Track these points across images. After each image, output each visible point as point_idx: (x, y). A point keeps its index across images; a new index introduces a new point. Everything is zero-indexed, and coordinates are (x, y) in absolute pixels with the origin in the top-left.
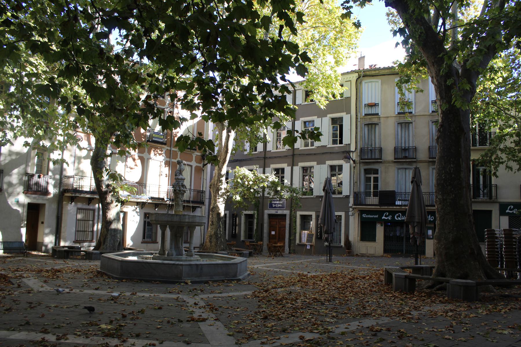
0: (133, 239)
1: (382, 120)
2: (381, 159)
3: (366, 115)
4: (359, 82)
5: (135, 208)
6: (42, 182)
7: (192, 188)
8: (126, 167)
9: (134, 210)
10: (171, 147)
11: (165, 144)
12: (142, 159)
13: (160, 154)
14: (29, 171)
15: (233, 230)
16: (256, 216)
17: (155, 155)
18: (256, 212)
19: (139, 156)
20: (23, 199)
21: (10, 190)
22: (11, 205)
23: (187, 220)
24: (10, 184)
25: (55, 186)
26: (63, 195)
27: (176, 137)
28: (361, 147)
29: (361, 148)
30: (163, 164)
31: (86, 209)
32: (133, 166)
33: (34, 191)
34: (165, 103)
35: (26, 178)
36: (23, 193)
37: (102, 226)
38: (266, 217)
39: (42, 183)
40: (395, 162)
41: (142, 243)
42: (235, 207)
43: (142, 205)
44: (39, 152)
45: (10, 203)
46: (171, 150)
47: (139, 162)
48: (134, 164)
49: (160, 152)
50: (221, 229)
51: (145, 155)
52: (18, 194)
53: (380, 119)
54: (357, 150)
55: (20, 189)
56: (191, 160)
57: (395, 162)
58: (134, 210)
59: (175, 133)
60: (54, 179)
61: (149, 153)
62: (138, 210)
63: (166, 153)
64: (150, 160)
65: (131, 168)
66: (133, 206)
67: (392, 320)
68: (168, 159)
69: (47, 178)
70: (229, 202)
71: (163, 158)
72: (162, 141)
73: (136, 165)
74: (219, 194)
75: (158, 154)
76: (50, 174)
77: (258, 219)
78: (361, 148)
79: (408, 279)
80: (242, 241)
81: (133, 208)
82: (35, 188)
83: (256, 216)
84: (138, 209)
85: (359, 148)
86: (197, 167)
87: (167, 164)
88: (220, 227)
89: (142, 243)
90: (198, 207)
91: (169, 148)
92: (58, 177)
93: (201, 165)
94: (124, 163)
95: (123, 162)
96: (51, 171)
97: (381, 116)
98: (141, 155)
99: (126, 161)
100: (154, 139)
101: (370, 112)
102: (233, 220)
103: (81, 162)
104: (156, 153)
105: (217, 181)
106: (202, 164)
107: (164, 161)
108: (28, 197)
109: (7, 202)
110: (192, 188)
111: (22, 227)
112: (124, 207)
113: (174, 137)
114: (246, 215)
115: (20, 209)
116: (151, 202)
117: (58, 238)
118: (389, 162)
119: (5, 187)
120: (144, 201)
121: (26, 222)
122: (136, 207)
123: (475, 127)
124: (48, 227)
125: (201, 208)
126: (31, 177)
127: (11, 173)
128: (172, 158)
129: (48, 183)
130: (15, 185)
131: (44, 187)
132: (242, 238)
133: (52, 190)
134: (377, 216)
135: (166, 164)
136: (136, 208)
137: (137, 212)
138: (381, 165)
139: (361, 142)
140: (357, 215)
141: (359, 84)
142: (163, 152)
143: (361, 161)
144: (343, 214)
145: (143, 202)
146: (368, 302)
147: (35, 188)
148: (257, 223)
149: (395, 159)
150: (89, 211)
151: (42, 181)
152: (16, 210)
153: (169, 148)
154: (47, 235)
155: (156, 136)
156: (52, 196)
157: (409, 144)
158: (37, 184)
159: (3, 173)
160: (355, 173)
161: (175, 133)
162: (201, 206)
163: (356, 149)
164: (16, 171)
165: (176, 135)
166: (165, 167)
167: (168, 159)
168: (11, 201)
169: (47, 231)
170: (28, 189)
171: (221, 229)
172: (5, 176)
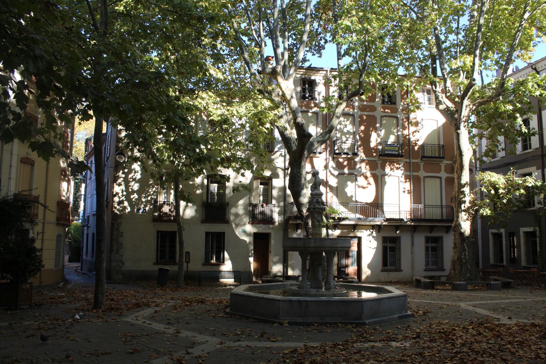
0: (369, 266)
5: (370, 233)
6: (268, 211)
7: (444, 204)
8: (357, 187)
9: (369, 235)
10: (410, 159)
11: (402, 156)
12: (375, 176)
13: (398, 168)
14: (254, 202)
15: (511, 253)
16: (538, 233)
17: (391, 169)
18: (537, 228)
19: (371, 174)
20: (249, 228)
21: (237, 221)
22: (239, 236)
23: (312, 245)
24: (237, 215)
25: (279, 214)
26: (288, 222)
27: (416, 146)
30: (403, 179)
32: (365, 185)
33: (259, 221)
34: (398, 110)
35: (251, 209)
36: (249, 223)
38: (522, 234)
39: (266, 211)
41: (382, 271)
42: (489, 223)
43: (378, 228)
44: (261, 181)
45: (237, 233)
46: (410, 162)
47: (371, 180)
48: (366, 182)
49: (398, 166)
50: (467, 253)
51: (378, 172)
52: (245, 224)
55: (246, 219)
56: (439, 171)
58: (369, 235)
59: (414, 142)
60: (279, 206)
61: (383, 169)
62: (374, 234)
63: (404, 166)
64: (386, 177)
65: (364, 188)
66: (368, 230)
68: (408, 173)
69: (270, 207)
70: (474, 218)
71: (402, 172)
72: (397, 153)
73: (369, 184)
74: (461, 208)
75: (395, 169)
76: (274, 202)
77: (541, 237)
80: (492, 265)
81: (368, 232)
82: (260, 217)
83: (538, 233)
84: (374, 233)
87: (407, 177)
88: (464, 250)
89: (382, 271)
91: (408, 160)
92: (282, 204)
94: (354, 183)
95: (352, 182)
96: (275, 199)
98: (374, 172)
99: (356, 180)
100: (386, 152)
102: (510, 240)
103: (385, 183)
104: (393, 167)
105: (458, 193)
107: (403, 176)
108: (254, 226)
109: (235, 233)
110: (444, 204)
111: (250, 256)
112: (358, 231)
113: (413, 147)
114: (526, 233)
115: (247, 239)
116: (387, 223)
117: (285, 268)
119: (232, 218)
120: (379, 223)
121: (253, 252)
122: (371, 231)
123: (365, 115)
124: (276, 255)
126: (255, 207)
127: (236, 205)
128: (413, 171)
129: (272, 211)
130: (242, 216)
131: (268, 216)
132: (523, 263)
133: (277, 218)
135: (406, 178)
136: (372, 232)
137: (373, 237)
142: (401, 166)
145: (377, 225)
146: (431, 341)
147: (260, 217)
148: (541, 244)
151: (267, 209)
152: (243, 240)
153: (408, 160)
154: (275, 263)
155: (389, 148)
156: (277, 224)
158: (263, 213)
159: (228, 205)
161: (414, 142)
164: (241, 202)
165: (416, 144)
166: (406, 182)
167: (408, 173)
168: (238, 232)
169: (276, 259)
170: (254, 220)
171: (467, 253)
172: (231, 209)
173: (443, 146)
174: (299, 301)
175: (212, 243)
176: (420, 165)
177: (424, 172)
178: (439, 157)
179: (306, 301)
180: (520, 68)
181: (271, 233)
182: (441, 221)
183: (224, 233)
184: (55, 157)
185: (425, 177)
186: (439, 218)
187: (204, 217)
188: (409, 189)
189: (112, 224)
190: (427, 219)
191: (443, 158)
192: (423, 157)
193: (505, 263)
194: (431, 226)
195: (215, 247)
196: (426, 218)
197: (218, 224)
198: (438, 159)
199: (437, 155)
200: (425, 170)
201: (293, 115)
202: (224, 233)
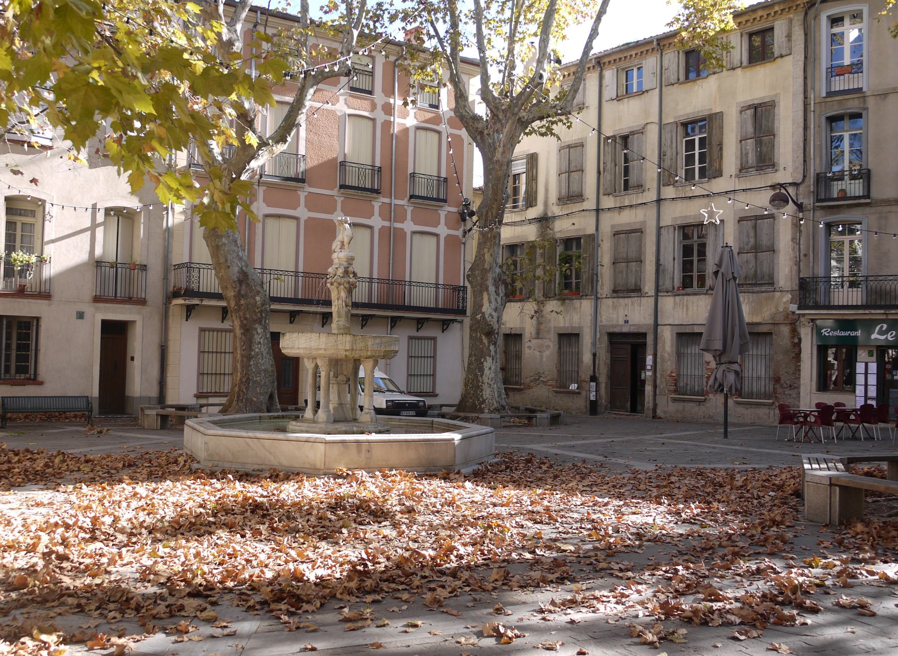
1: (871, 103)
2: (868, 197)
4: (813, 16)
28: (818, 171)
29: (818, 175)
31: (218, 330)
37: (645, 361)
53: (865, 102)
54: (807, 179)
67: (870, 578)
78: (818, 175)
79: (837, 489)
85: (812, 175)
86: (448, 238)
90: (453, 321)
91: (387, 200)
93: (459, 233)
97: (869, 93)
106: (461, 230)
125: (461, 322)
138: (867, 210)
139: (818, 160)
141: (813, 22)
143: (817, 204)
150: (224, 333)
153: (387, 200)
157: (601, 78)
162: (459, 318)
163: (804, 176)
173: (446, 179)
174: (357, 442)
175: (9, 337)
176: (406, 210)
177: (412, 223)
178: (438, 200)
179: (369, 442)
180: (475, 31)
182: (435, 310)
183: (38, 319)
185: (414, 233)
186: (432, 305)
188: (47, 223)
190: (301, 299)
191: (445, 201)
192: (411, 197)
194: (363, 316)
195: (14, 346)
196: (201, 290)
197: (26, 300)
199: (368, 186)
200: (415, 221)
202: (38, 319)
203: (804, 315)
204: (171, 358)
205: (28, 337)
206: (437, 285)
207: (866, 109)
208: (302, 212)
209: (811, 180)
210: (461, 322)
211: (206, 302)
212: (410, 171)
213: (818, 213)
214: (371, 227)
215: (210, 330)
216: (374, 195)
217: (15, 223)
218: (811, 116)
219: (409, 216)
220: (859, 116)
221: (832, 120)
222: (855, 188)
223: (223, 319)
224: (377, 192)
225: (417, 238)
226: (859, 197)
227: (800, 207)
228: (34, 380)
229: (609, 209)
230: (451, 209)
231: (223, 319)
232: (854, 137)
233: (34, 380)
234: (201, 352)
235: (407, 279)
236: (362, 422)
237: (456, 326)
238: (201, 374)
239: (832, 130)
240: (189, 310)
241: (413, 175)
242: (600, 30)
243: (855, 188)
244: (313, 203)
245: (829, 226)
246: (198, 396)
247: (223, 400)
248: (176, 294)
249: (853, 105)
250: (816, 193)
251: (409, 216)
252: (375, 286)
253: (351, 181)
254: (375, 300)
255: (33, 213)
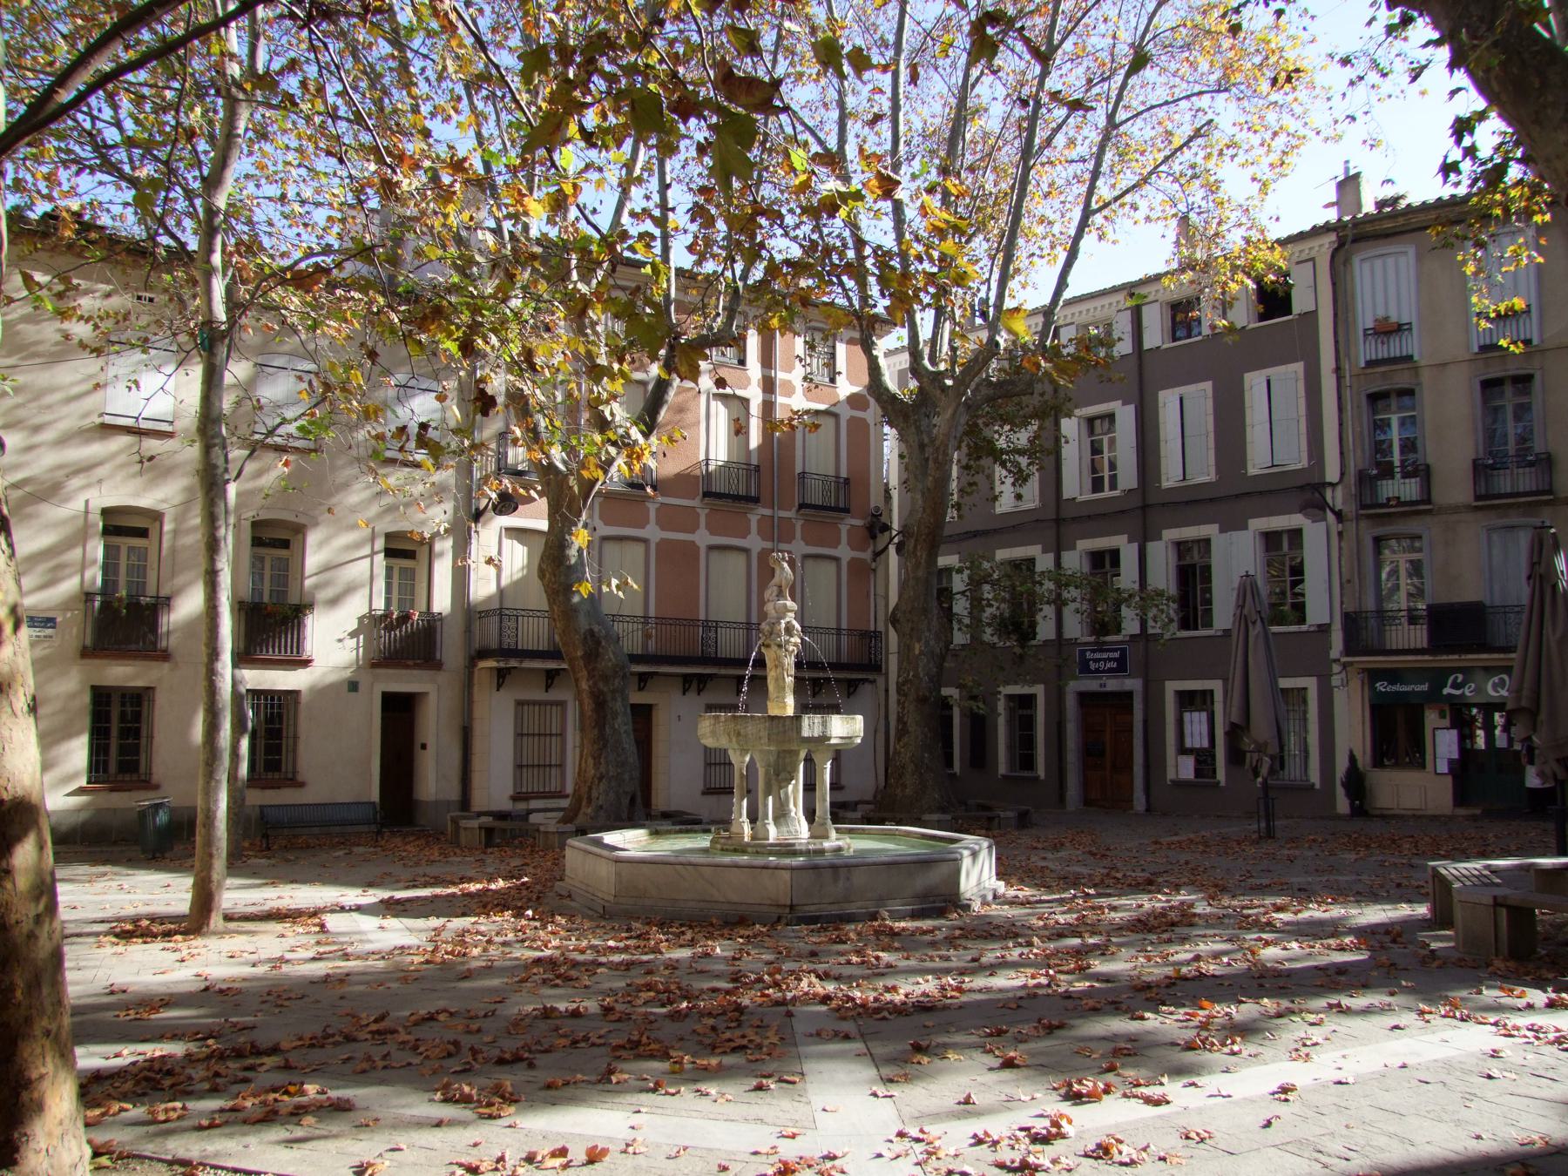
1: (1426, 377)
2: (1428, 501)
3: (1370, 364)
28: (1361, 467)
40: (1477, 508)
41: (704, 793)
53: (1417, 375)
54: (1346, 477)
57: (1477, 508)
86: (853, 563)
89: (704, 793)
91: (767, 512)
93: (867, 555)
97: (1423, 363)
101: (1383, 353)
106: (870, 551)
114: (1010, 697)
118: (1456, 509)
134: (1425, 687)
138: (1428, 519)
139: (1359, 452)
140: (1356, 684)
144: (1310, 683)
149: (1478, 498)
153: (767, 512)
160: (1345, 552)
162: (871, 677)
163: (1342, 474)
173: (847, 481)
178: (836, 509)
181: (425, 694)
184: (1452, 72)
185: (711, 548)
187: (242, 646)
189: (1022, 904)
191: (847, 510)
192: (802, 506)
193: (957, 767)
198: (834, 514)
201: (710, 346)
203: (1351, 664)
204: (478, 745)
205: (137, 717)
206: (839, 630)
207: (1419, 384)
208: (653, 532)
209: (1351, 478)
210: (873, 682)
211: (528, 664)
212: (798, 470)
213: (1363, 524)
214: (836, 559)
215: (528, 703)
216: (751, 505)
217: (118, 548)
218: (1347, 394)
219: (703, 520)
220: (1410, 392)
221: (1374, 398)
222: (1408, 489)
223: (548, 688)
224: (756, 500)
225: (715, 555)
226: (1412, 503)
227: (1339, 515)
228: (294, 782)
229: (1074, 519)
230: (851, 523)
231: (548, 688)
232: (1402, 422)
233: (294, 782)
234: (519, 735)
235: (702, 617)
236: (1384, 817)
237: (868, 687)
238: (519, 767)
239: (1375, 412)
240: (502, 676)
241: (803, 475)
242: (1069, 280)
243: (1408, 489)
244: (668, 518)
245: (1378, 541)
246: (516, 798)
247: (565, 803)
248: (483, 654)
249: (1402, 380)
250: (1360, 495)
251: (703, 520)
252: (844, 639)
253: (815, 498)
254: (844, 659)
255: (285, 544)
